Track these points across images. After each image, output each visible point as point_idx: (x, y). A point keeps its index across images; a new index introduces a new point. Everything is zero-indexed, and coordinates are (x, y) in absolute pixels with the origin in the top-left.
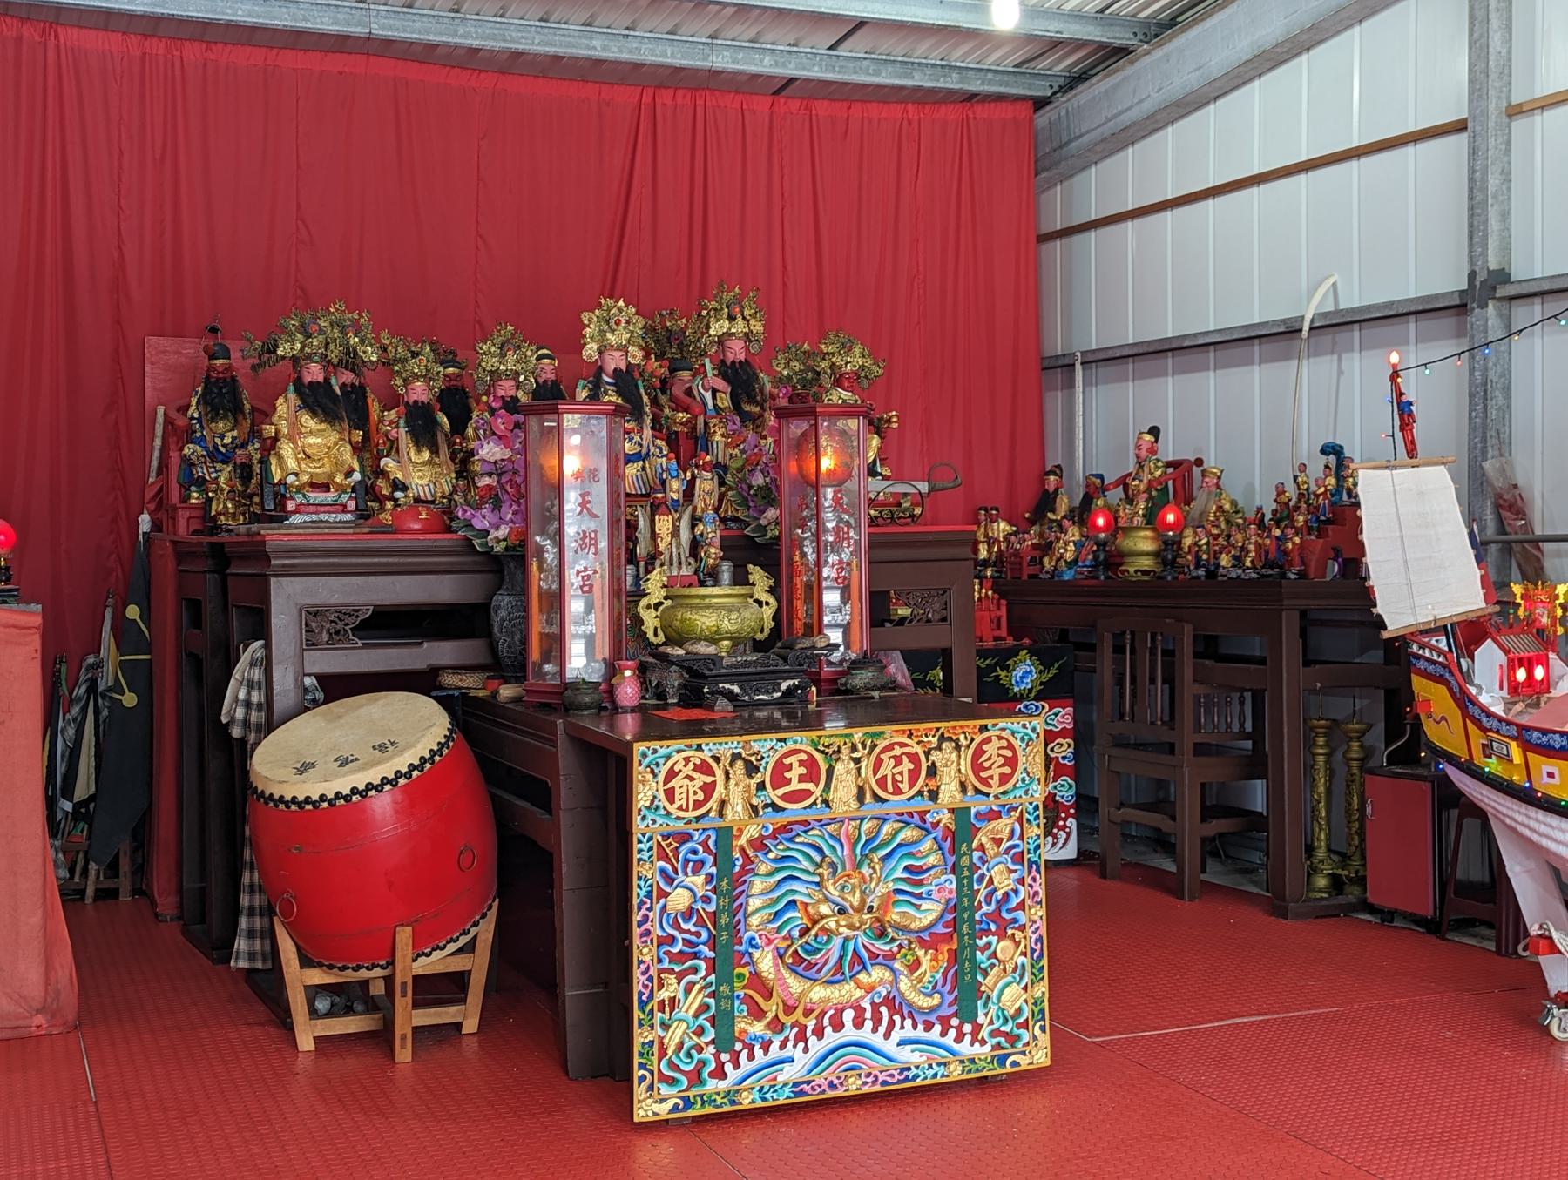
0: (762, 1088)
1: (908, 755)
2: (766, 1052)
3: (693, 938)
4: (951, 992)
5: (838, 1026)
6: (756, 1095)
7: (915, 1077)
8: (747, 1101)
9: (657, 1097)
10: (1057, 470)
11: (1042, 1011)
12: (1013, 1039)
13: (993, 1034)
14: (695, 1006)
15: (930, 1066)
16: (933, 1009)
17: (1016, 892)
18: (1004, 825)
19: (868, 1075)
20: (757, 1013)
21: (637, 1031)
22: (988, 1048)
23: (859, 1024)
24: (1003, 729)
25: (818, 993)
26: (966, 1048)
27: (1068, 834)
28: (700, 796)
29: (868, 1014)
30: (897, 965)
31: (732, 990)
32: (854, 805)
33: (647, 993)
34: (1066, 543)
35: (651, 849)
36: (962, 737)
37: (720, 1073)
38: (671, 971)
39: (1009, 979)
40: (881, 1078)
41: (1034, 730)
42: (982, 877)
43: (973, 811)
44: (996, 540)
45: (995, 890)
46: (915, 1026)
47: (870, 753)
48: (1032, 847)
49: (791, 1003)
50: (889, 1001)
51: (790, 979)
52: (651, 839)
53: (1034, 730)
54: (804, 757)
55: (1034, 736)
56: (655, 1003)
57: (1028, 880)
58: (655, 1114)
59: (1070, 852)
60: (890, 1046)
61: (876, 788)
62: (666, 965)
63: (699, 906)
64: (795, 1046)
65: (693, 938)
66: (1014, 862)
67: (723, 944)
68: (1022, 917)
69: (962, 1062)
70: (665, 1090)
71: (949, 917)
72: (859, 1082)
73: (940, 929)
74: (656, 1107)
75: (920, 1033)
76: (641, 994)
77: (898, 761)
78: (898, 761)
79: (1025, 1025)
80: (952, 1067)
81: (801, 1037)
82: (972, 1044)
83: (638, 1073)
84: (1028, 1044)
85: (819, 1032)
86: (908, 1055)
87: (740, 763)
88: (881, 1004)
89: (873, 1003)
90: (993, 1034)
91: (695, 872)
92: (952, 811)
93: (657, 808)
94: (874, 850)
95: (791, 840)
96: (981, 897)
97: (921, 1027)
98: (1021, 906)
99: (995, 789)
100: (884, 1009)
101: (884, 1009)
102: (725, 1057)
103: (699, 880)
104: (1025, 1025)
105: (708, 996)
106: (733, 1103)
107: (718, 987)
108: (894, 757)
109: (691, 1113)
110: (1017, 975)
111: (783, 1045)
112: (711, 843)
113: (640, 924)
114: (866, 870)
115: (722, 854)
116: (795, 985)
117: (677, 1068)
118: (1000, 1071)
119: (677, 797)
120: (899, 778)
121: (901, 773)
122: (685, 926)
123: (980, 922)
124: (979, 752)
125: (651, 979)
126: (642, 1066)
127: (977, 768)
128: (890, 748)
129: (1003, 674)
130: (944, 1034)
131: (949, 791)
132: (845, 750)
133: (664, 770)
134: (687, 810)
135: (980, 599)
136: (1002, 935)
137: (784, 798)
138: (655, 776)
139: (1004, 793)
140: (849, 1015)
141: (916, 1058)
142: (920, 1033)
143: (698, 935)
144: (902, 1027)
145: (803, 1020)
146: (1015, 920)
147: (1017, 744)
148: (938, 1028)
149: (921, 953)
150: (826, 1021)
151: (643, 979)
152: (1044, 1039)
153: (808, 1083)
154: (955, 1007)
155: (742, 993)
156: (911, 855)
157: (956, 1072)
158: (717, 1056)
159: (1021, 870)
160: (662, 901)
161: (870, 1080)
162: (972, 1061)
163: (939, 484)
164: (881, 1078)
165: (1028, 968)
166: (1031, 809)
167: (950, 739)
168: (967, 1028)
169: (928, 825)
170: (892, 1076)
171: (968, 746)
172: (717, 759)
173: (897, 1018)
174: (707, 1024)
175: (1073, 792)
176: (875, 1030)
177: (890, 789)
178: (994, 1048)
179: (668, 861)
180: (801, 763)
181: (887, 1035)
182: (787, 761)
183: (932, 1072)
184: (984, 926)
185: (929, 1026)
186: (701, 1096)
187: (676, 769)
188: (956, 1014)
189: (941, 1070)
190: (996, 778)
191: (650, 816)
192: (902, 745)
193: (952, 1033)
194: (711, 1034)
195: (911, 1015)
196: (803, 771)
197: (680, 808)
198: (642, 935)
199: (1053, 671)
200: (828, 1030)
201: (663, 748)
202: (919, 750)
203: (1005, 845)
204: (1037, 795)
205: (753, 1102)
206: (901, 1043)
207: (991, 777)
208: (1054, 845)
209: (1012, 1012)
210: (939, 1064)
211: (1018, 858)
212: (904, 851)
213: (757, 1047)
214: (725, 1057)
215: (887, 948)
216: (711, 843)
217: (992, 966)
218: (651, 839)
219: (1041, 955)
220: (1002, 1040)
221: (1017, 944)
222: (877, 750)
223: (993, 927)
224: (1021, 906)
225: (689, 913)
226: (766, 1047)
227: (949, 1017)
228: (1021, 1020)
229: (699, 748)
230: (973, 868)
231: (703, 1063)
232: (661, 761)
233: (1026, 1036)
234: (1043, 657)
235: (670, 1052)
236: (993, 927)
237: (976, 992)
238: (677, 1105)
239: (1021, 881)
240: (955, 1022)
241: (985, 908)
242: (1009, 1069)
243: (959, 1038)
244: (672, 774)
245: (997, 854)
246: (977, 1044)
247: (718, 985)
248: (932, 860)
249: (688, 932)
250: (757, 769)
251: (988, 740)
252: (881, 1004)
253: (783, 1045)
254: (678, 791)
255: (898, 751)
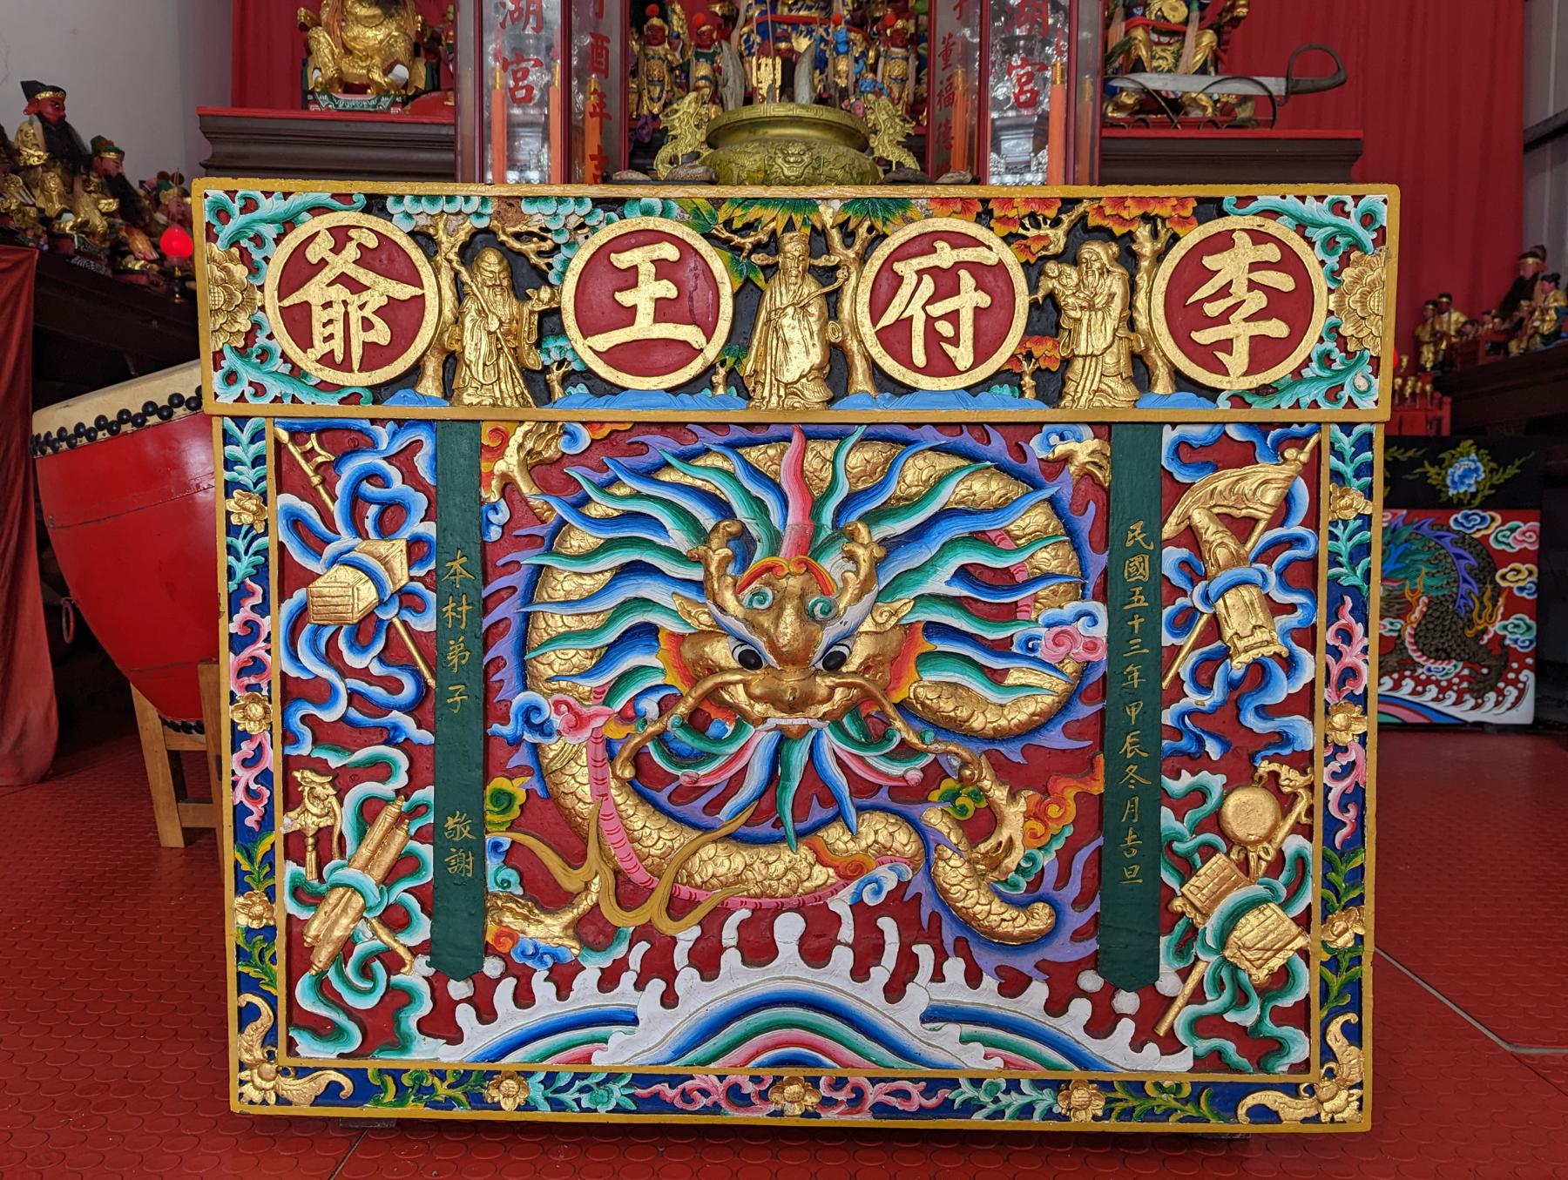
0: (551, 1077)
1: (975, 268)
2: (563, 992)
3: (378, 692)
4: (1081, 902)
5: (759, 950)
6: (537, 1092)
7: (970, 1107)
8: (507, 1101)
9: (283, 1059)
10: (1540, 252)
11: (1355, 986)
12: (1263, 1049)
13: (1201, 1026)
14: (388, 858)
15: (1013, 1086)
16: (1029, 942)
17: (1289, 664)
18: (1262, 484)
19: (839, 1083)
20: (548, 897)
21: (233, 901)
22: (1181, 1063)
23: (815, 951)
24: (1273, 214)
25: (718, 862)
26: (1117, 1051)
27: (1522, 693)
28: (381, 334)
29: (847, 933)
30: (934, 818)
31: (480, 827)
32: (815, 393)
33: (257, 810)
34: (1544, 311)
35: (258, 460)
36: (1143, 232)
37: (442, 1025)
38: (320, 767)
39: (1257, 890)
40: (873, 1094)
41: (1368, 219)
42: (1190, 614)
43: (1169, 436)
44: (1445, 335)
45: (1225, 654)
46: (973, 977)
47: (863, 259)
48: (1344, 547)
49: (640, 876)
50: (901, 904)
51: (640, 819)
52: (257, 436)
53: (1368, 219)
54: (669, 252)
55: (1368, 237)
56: (276, 838)
57: (1327, 636)
58: (281, 1100)
59: (1523, 714)
60: (904, 1019)
61: (877, 352)
62: (305, 749)
63: (389, 614)
64: (640, 985)
65: (378, 692)
66: (1286, 584)
67: (463, 717)
68: (1305, 734)
69: (1106, 1086)
70: (309, 1048)
71: (1084, 711)
72: (811, 1100)
73: (1055, 739)
74: (290, 1086)
75: (987, 995)
76: (240, 812)
77: (946, 284)
78: (946, 284)
79: (1300, 1016)
80: (1079, 1096)
81: (659, 965)
82: (1137, 1044)
83: (235, 1001)
84: (1305, 1066)
85: (707, 961)
86: (949, 1047)
87: (491, 261)
88: (881, 910)
89: (858, 906)
90: (1201, 1026)
91: (385, 530)
92: (1103, 429)
93: (265, 355)
94: (872, 519)
95: (649, 474)
96: (1183, 667)
97: (990, 983)
98: (1303, 702)
99: (1236, 376)
100: (887, 925)
101: (887, 925)
102: (458, 989)
103: (396, 550)
104: (1300, 1016)
105: (420, 836)
106: (477, 1101)
107: (440, 818)
108: (934, 271)
109: (368, 1111)
110: (1280, 883)
111: (608, 980)
112: (422, 462)
113: (237, 644)
114: (832, 564)
115: (454, 492)
116: (656, 835)
117: (336, 1001)
118: (1216, 1126)
119: (318, 332)
120: (945, 328)
121: (953, 317)
122: (354, 661)
123: (1177, 733)
124: (1192, 273)
125: (265, 778)
126: (245, 984)
127: (1184, 316)
128: (924, 244)
129: (1432, 471)
130: (1056, 1006)
131: (1098, 385)
132: (793, 247)
133: (280, 255)
134: (346, 366)
135: (1413, 394)
136: (1241, 774)
137: (610, 357)
138: (254, 270)
139: (1264, 391)
140: (789, 929)
141: (974, 1058)
142: (987, 995)
143: (394, 686)
144: (938, 976)
145: (665, 925)
146: (1283, 738)
147: (1311, 258)
148: (1039, 991)
149: (1000, 794)
150: (729, 935)
151: (246, 776)
152: (1355, 1061)
153: (674, 1080)
154: (1091, 946)
155: (506, 841)
156: (977, 539)
157: (1085, 1110)
158: (437, 986)
159: (1306, 609)
160: (299, 595)
161: (841, 1096)
162: (1137, 1088)
163: (1306, 82)
164: (873, 1094)
165: (1315, 869)
166: (1346, 443)
167: (1105, 234)
168: (1127, 1002)
169: (1032, 466)
170: (905, 1095)
171: (1159, 257)
172: (424, 239)
173: (925, 953)
174: (413, 903)
175: (1532, 635)
176: (860, 972)
177: (920, 359)
178: (1200, 1063)
179: (308, 494)
180: (663, 269)
181: (895, 990)
182: (623, 260)
183: (1017, 1100)
184: (1184, 743)
185: (1013, 985)
186: (396, 1074)
187: (313, 255)
188: (1093, 962)
189: (1045, 1099)
190: (1242, 349)
191: (247, 374)
192: (959, 240)
193: (1081, 1009)
194: (422, 930)
195: (962, 949)
196: (667, 289)
197: (327, 360)
198: (241, 672)
199: (1511, 471)
200: (731, 959)
201: (273, 198)
202: (1010, 257)
203: (1260, 537)
204: (1366, 404)
205: (527, 1106)
206: (935, 1015)
207: (1227, 345)
208: (1497, 704)
209: (1261, 975)
210: (1039, 1084)
211: (1302, 575)
212: (959, 528)
213: (540, 975)
214: (458, 989)
215: (896, 770)
216: (422, 462)
217: (1208, 851)
218: (257, 436)
219: (1358, 838)
220: (1230, 1047)
221: (1286, 802)
222: (883, 252)
223: (1213, 749)
224: (1303, 702)
225: (364, 630)
226: (563, 978)
227: (1079, 966)
228: (1288, 1002)
229: (376, 205)
230: (1163, 590)
231: (399, 998)
232: (270, 231)
233: (1301, 1047)
234: (1498, 454)
235: (322, 956)
236: (1213, 749)
237: (1160, 911)
238: (333, 1089)
239: (1307, 636)
240: (1090, 981)
241: (1193, 699)
242: (1242, 1124)
243: (1102, 1024)
244: (299, 271)
245: (1237, 560)
246: (1152, 1049)
247: (442, 812)
248: (1046, 559)
249: (364, 674)
250: (542, 277)
251: (1223, 242)
252: (881, 910)
253: (608, 980)
254: (319, 316)
255: (945, 256)
